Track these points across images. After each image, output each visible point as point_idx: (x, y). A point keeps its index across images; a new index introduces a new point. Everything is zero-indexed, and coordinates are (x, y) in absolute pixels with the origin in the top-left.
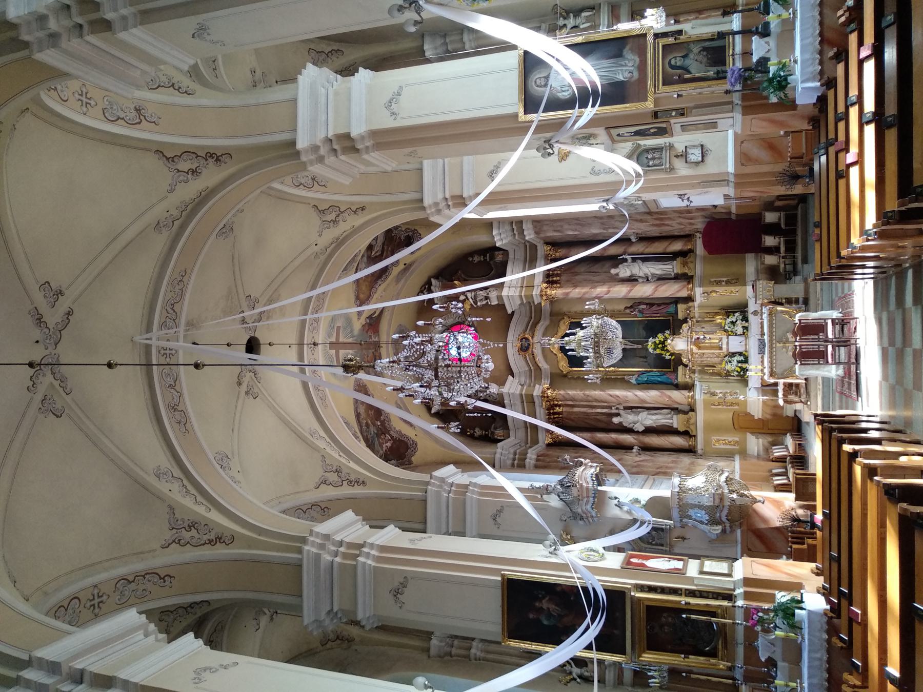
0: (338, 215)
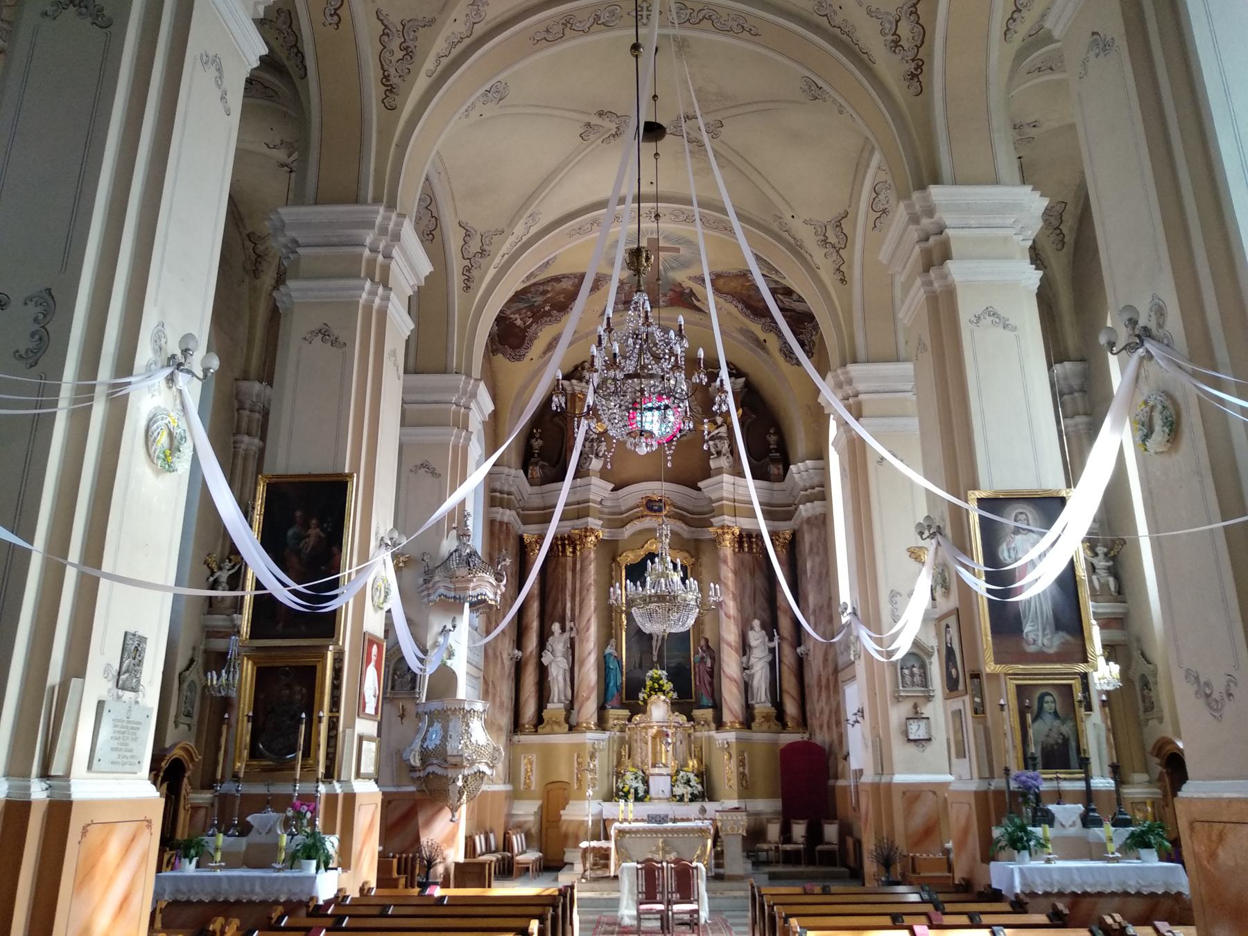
0: (834, 247)
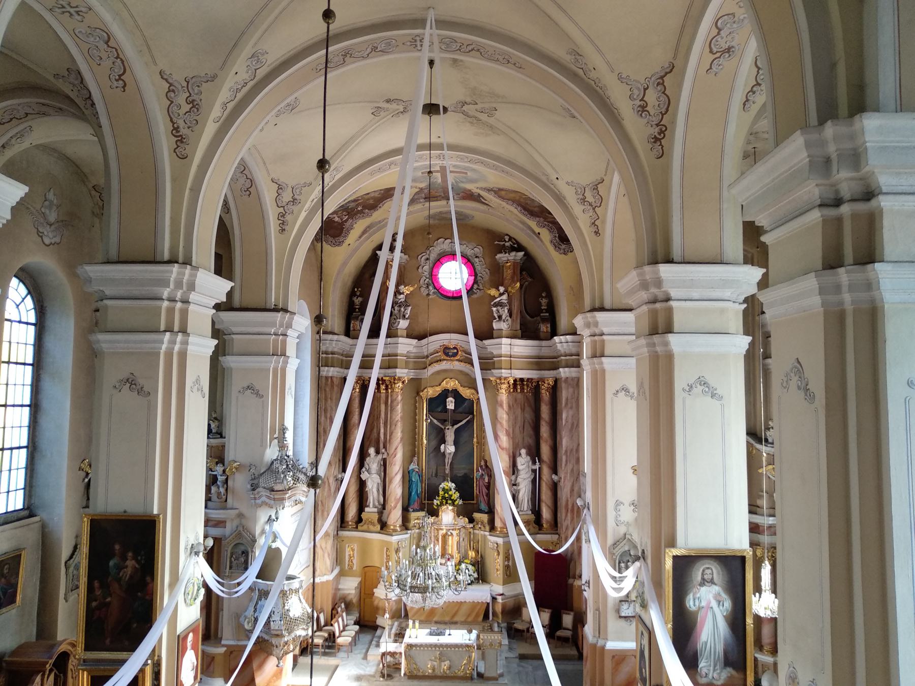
0: (591, 205)
